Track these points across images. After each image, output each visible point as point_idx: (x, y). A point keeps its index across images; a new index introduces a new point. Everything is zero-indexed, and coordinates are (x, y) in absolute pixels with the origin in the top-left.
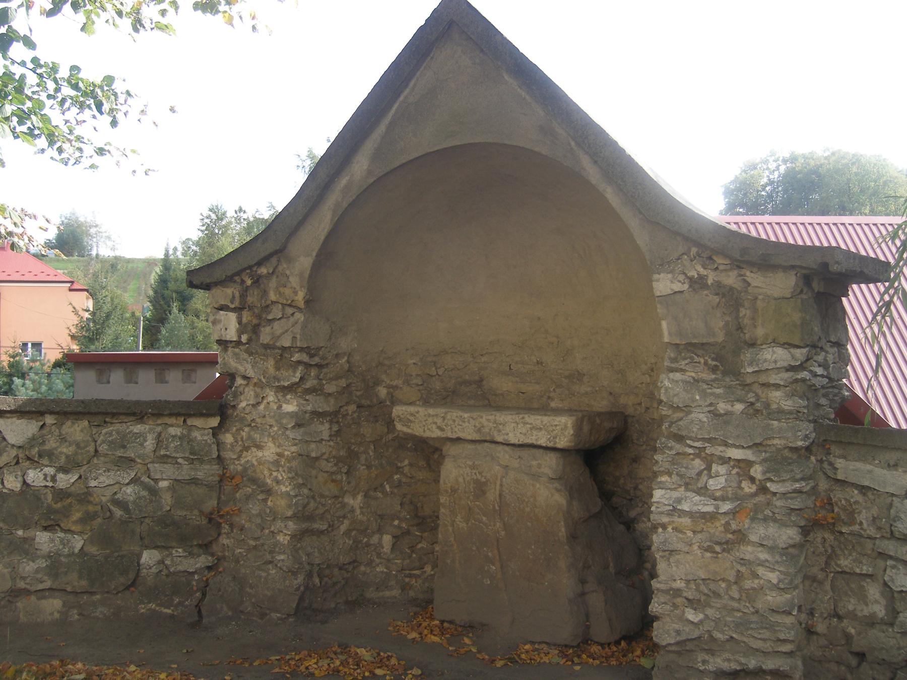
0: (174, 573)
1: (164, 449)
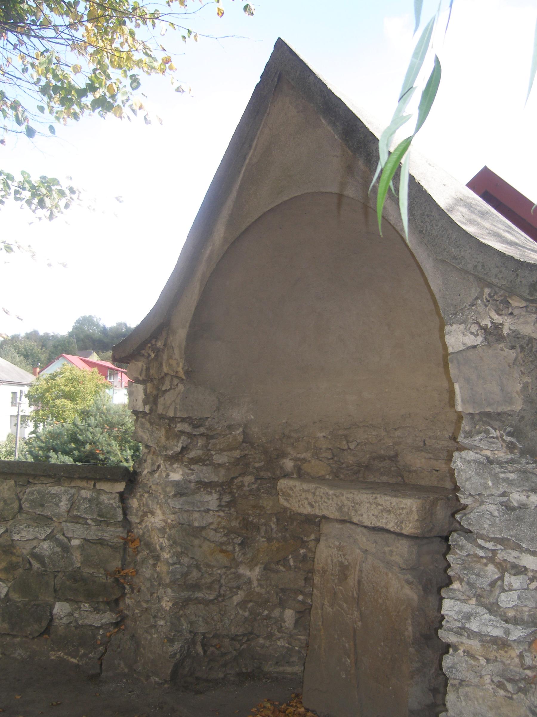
0: (82, 626)
1: (76, 509)
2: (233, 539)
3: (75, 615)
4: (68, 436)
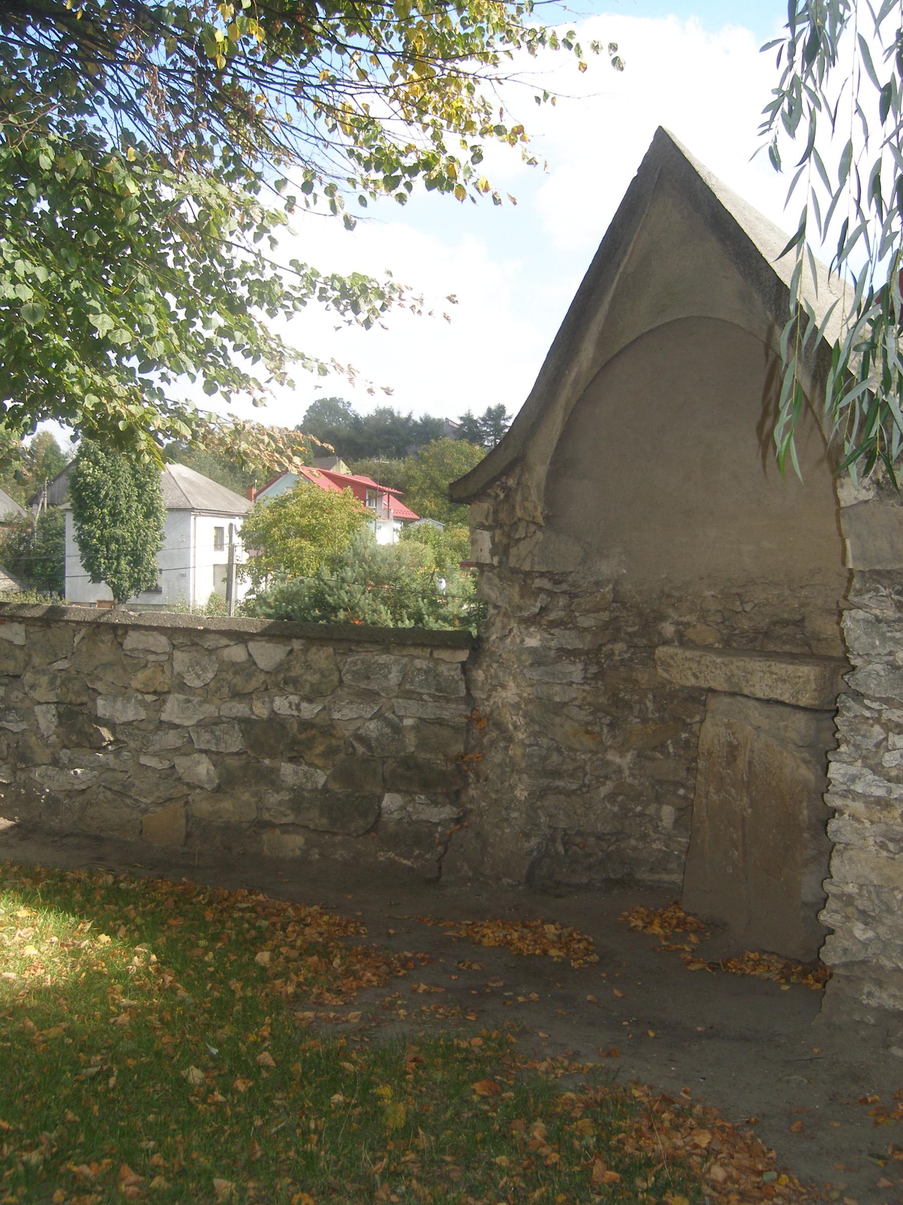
0: (417, 822)
2: (600, 719)
3: (408, 809)
4: (310, 598)
